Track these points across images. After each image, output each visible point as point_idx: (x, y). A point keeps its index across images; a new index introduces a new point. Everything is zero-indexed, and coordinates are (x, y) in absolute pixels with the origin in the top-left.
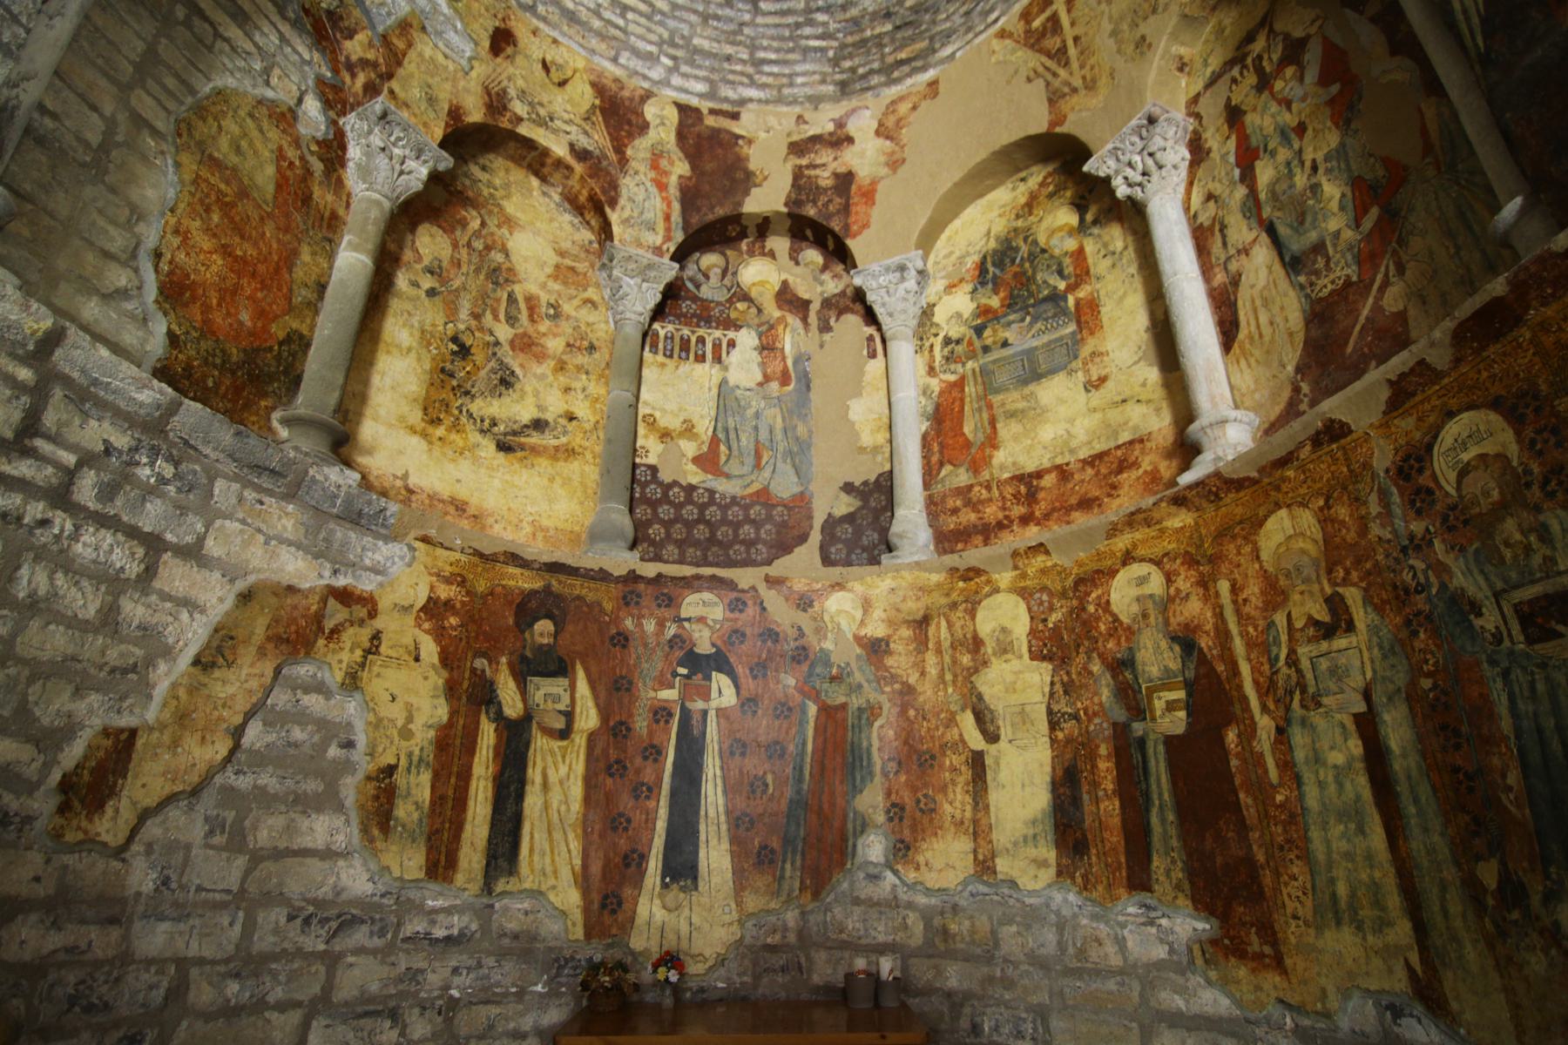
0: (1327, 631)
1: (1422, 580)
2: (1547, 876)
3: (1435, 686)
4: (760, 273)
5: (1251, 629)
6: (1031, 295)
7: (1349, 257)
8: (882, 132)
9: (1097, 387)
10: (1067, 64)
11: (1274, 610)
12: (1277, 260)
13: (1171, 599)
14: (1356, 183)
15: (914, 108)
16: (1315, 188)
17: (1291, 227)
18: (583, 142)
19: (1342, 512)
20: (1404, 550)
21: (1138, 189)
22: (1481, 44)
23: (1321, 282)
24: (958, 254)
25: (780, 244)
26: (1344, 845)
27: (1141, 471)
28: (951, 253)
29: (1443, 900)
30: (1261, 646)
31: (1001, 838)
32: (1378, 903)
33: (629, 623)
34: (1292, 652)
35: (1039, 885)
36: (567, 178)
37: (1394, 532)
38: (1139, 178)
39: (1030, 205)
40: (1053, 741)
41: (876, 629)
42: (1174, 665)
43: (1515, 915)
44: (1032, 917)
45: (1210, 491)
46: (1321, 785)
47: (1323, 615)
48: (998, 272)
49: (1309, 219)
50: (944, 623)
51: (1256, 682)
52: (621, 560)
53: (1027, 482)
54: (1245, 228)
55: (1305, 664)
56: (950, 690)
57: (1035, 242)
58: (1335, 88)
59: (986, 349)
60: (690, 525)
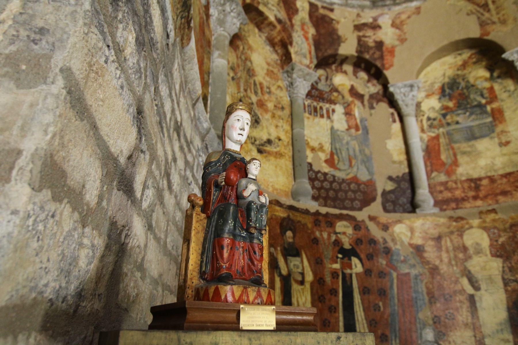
4: (342, 80)
6: (468, 103)
8: (394, 25)
15: (409, 17)
18: (279, 16)
25: (348, 68)
33: (318, 234)
36: (272, 30)
39: (464, 65)
40: (506, 291)
41: (419, 242)
48: (451, 92)
50: (448, 240)
52: (313, 206)
53: (475, 183)
57: (468, 82)
59: (448, 124)
60: (327, 190)
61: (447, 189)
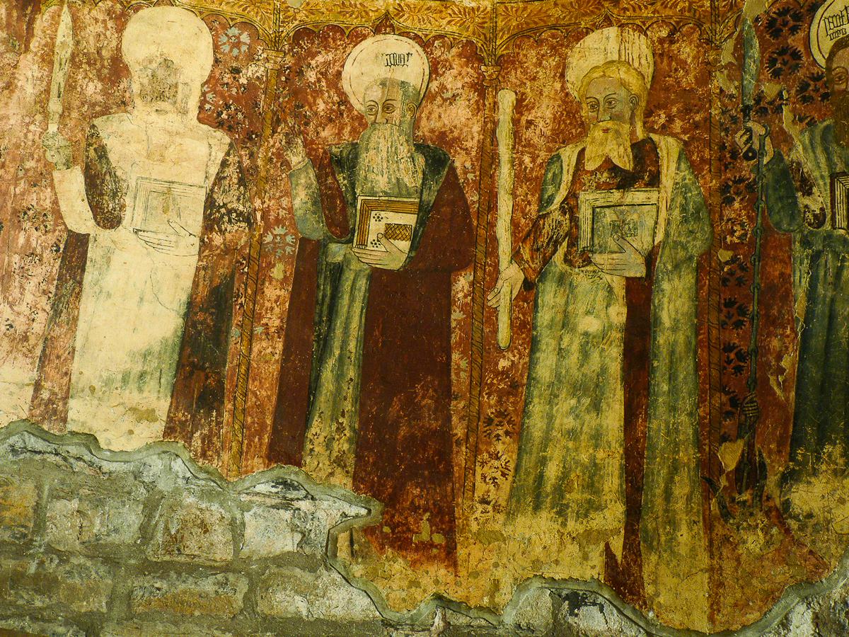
0: (625, 181)
1: (756, 146)
2: (792, 459)
3: (734, 260)
5: (527, 159)
11: (565, 142)
13: (429, 96)
19: (687, 51)
20: (746, 110)
26: (570, 422)
29: (670, 481)
30: (534, 183)
31: (85, 369)
32: (592, 486)
34: (572, 195)
35: (132, 445)
37: (742, 88)
40: (204, 245)
42: (411, 181)
43: (746, 496)
44: (106, 488)
46: (561, 353)
47: (625, 161)
50: (66, 18)
51: (514, 224)
55: (585, 213)
56: (53, 128)
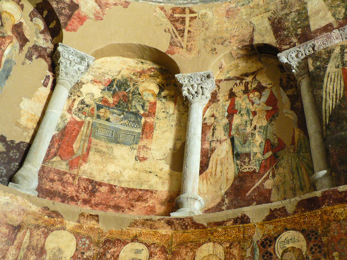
7: (257, 163)
9: (141, 160)
10: (182, 36)
12: (231, 151)
14: (267, 141)
16: (253, 135)
17: (240, 143)
19: (235, 251)
21: (192, 96)
22: (327, 121)
23: (245, 167)
24: (103, 70)
27: (147, 204)
28: (100, 68)
38: (194, 93)
39: (141, 73)
45: (185, 224)
49: (247, 143)
50: (28, 234)
53: (93, 186)
54: (223, 134)
58: (270, 108)
59: (99, 117)
61: (61, 180)
